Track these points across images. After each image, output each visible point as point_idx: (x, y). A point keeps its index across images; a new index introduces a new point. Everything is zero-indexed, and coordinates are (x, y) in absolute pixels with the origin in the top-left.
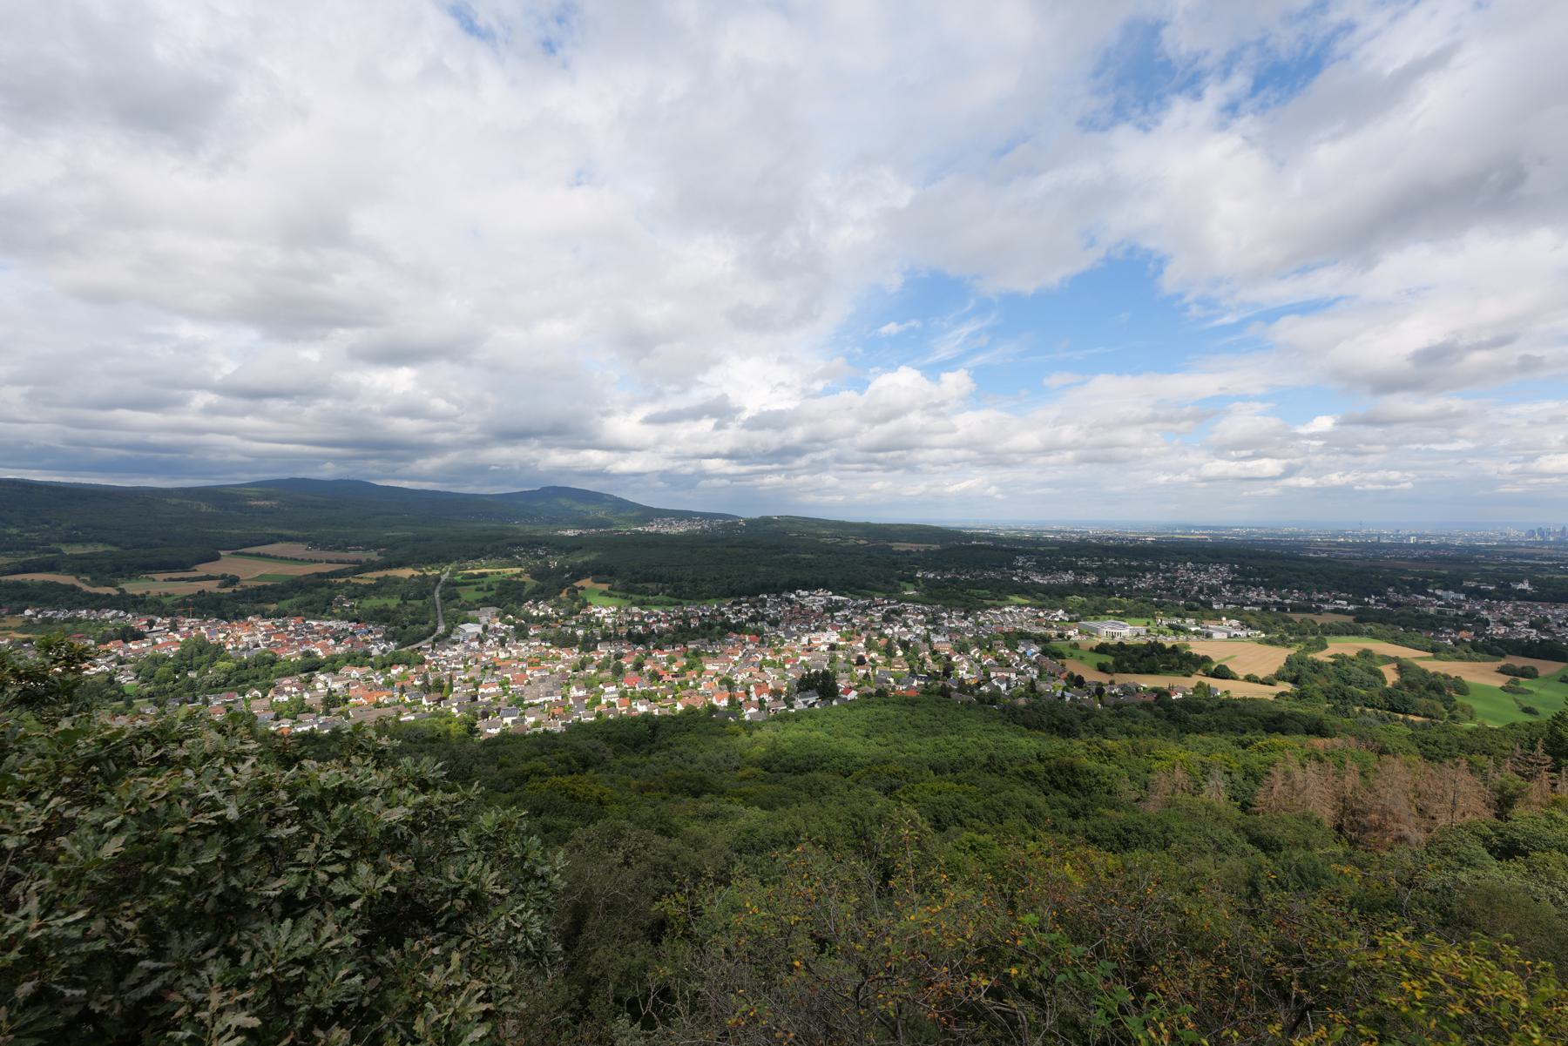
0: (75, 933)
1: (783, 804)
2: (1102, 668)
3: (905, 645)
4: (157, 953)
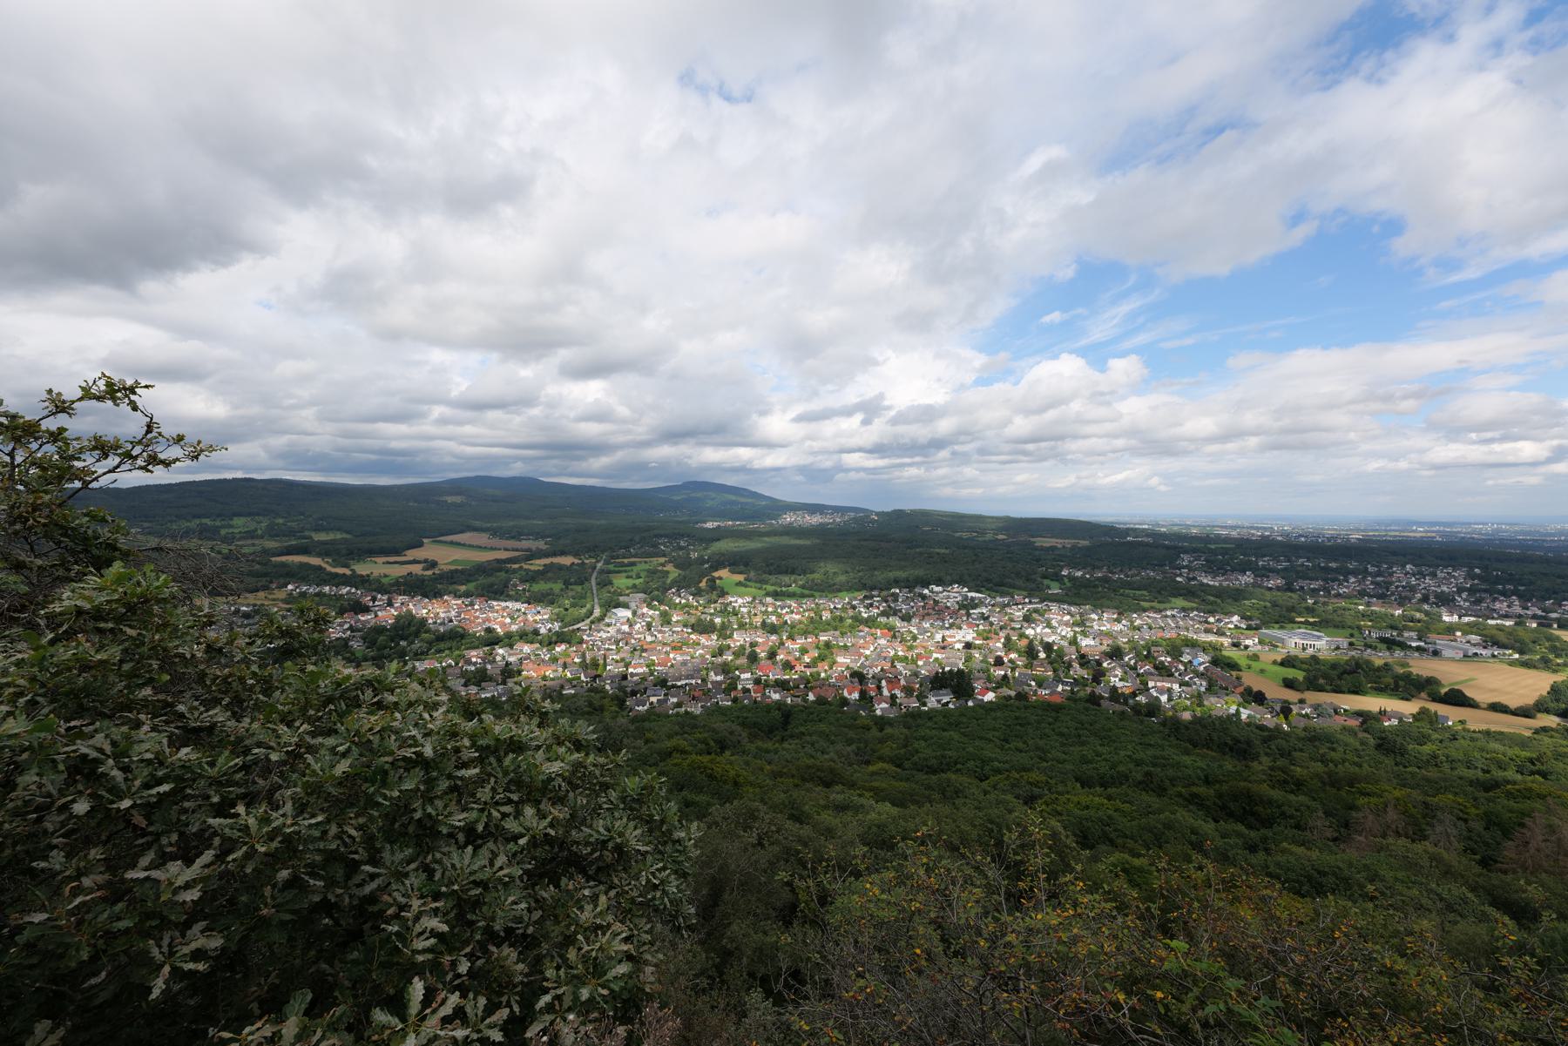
0: (317, 834)
1: (916, 802)
2: (1289, 684)
3: (1048, 647)
4: (374, 861)
